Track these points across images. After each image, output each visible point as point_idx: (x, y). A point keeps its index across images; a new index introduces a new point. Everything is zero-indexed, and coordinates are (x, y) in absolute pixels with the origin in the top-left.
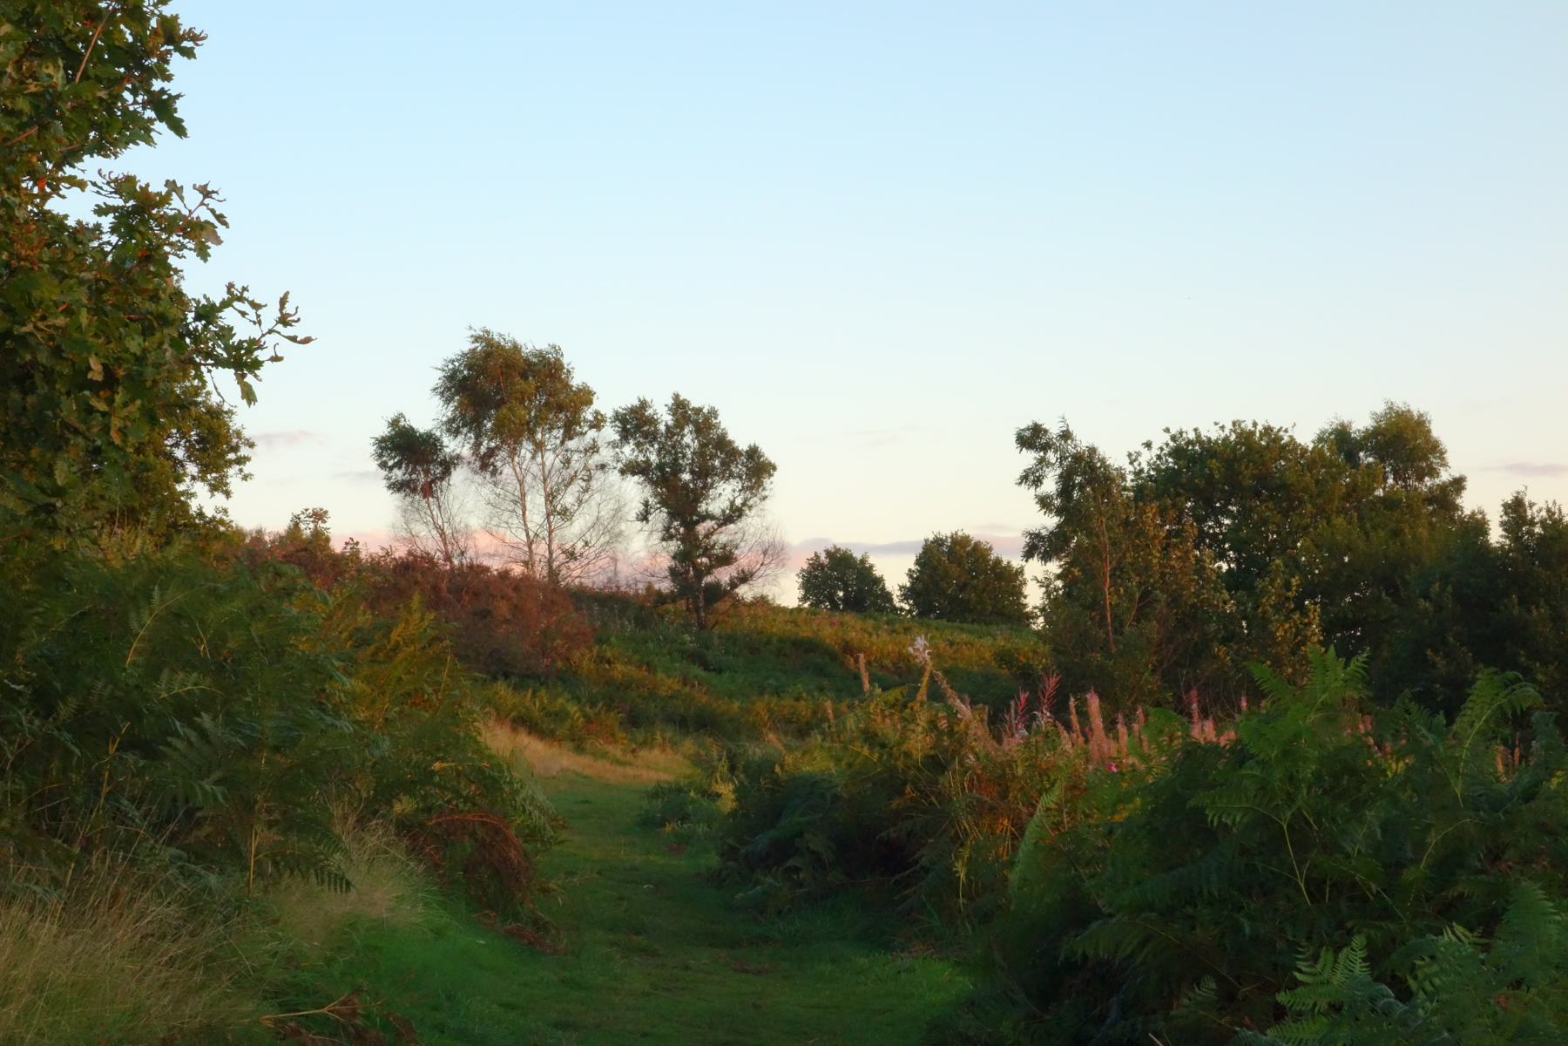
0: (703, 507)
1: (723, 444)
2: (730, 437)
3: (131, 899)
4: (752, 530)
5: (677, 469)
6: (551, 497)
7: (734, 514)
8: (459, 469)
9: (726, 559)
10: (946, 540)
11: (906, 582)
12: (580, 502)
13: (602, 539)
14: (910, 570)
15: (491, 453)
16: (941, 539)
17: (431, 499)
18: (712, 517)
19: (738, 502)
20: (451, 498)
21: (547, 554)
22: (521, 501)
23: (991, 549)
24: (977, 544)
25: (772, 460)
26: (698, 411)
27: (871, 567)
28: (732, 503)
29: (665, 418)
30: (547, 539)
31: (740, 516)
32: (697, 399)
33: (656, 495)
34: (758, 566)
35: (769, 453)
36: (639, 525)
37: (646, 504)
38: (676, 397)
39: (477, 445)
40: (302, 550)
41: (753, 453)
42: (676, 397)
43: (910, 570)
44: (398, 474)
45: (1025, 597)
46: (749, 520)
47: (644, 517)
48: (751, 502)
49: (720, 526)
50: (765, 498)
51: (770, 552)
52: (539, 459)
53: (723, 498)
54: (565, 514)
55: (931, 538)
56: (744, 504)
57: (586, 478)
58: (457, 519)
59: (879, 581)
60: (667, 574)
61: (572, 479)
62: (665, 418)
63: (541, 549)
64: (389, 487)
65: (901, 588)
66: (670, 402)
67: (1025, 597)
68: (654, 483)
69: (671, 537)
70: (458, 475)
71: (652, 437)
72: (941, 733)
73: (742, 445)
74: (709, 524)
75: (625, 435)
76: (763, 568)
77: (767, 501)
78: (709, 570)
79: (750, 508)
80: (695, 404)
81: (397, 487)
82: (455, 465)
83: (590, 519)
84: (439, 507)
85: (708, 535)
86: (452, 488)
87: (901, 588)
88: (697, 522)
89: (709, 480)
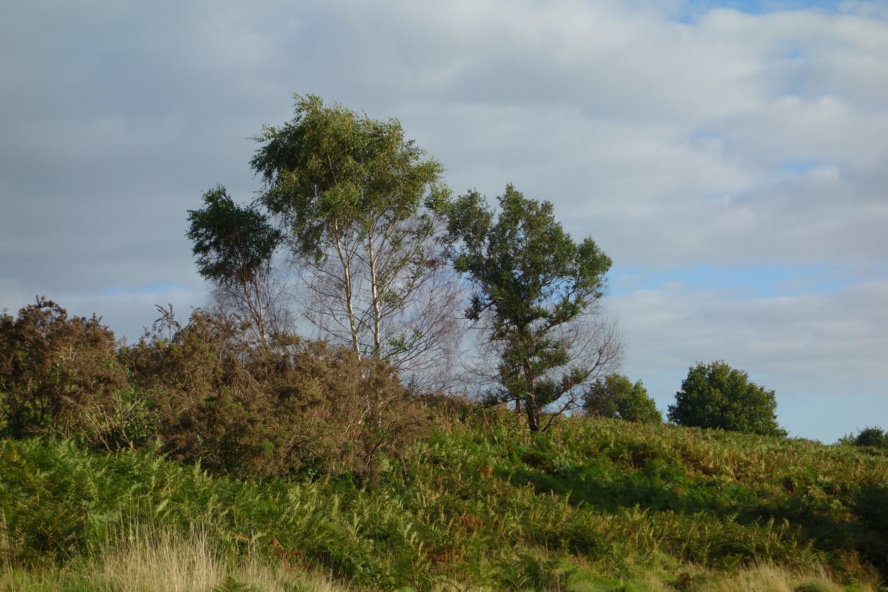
0: (535, 305)
1: (555, 237)
2: (565, 231)
3: (189, 569)
4: (585, 328)
5: (507, 263)
6: (381, 280)
7: (567, 312)
8: (278, 248)
9: (559, 359)
10: (708, 369)
11: (674, 402)
12: (410, 287)
13: (434, 328)
14: (678, 393)
15: (316, 232)
16: (704, 368)
17: (248, 284)
18: (544, 315)
19: (572, 299)
20: (271, 282)
21: (373, 344)
22: (345, 285)
23: (746, 376)
24: (735, 372)
25: (609, 254)
26: (532, 205)
27: (645, 391)
28: (566, 300)
29: (495, 211)
30: (373, 328)
31: (573, 314)
32: (530, 192)
33: (485, 290)
34: (594, 364)
35: (603, 247)
36: (470, 322)
37: (476, 301)
38: (510, 189)
39: (301, 218)
40: (46, 305)
41: (588, 249)
42: (510, 189)
43: (678, 393)
44: (213, 257)
45: (775, 417)
46: (583, 318)
47: (473, 314)
48: (586, 299)
49: (553, 324)
50: (599, 296)
51: (605, 351)
52: (366, 241)
53: (554, 295)
54: (394, 301)
55: (695, 367)
56: (577, 302)
57: (417, 261)
58: (277, 305)
59: (649, 404)
60: (497, 373)
61: (404, 261)
62: (495, 211)
63: (367, 338)
64: (203, 272)
65: (671, 408)
66: (502, 192)
67: (775, 417)
68: (486, 280)
69: (502, 335)
70: (280, 254)
71: (480, 231)
72: (574, 519)
73: (578, 241)
74: (541, 322)
75: (454, 228)
76: (598, 367)
77: (602, 299)
78: (539, 370)
79: (584, 305)
80: (527, 197)
81: (210, 271)
82: (274, 245)
83: (421, 307)
84: (257, 292)
85: (540, 333)
86: (272, 271)
87: (671, 408)
88: (530, 320)
89: (541, 277)
